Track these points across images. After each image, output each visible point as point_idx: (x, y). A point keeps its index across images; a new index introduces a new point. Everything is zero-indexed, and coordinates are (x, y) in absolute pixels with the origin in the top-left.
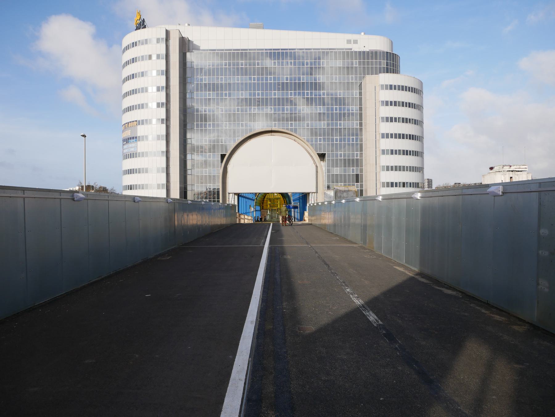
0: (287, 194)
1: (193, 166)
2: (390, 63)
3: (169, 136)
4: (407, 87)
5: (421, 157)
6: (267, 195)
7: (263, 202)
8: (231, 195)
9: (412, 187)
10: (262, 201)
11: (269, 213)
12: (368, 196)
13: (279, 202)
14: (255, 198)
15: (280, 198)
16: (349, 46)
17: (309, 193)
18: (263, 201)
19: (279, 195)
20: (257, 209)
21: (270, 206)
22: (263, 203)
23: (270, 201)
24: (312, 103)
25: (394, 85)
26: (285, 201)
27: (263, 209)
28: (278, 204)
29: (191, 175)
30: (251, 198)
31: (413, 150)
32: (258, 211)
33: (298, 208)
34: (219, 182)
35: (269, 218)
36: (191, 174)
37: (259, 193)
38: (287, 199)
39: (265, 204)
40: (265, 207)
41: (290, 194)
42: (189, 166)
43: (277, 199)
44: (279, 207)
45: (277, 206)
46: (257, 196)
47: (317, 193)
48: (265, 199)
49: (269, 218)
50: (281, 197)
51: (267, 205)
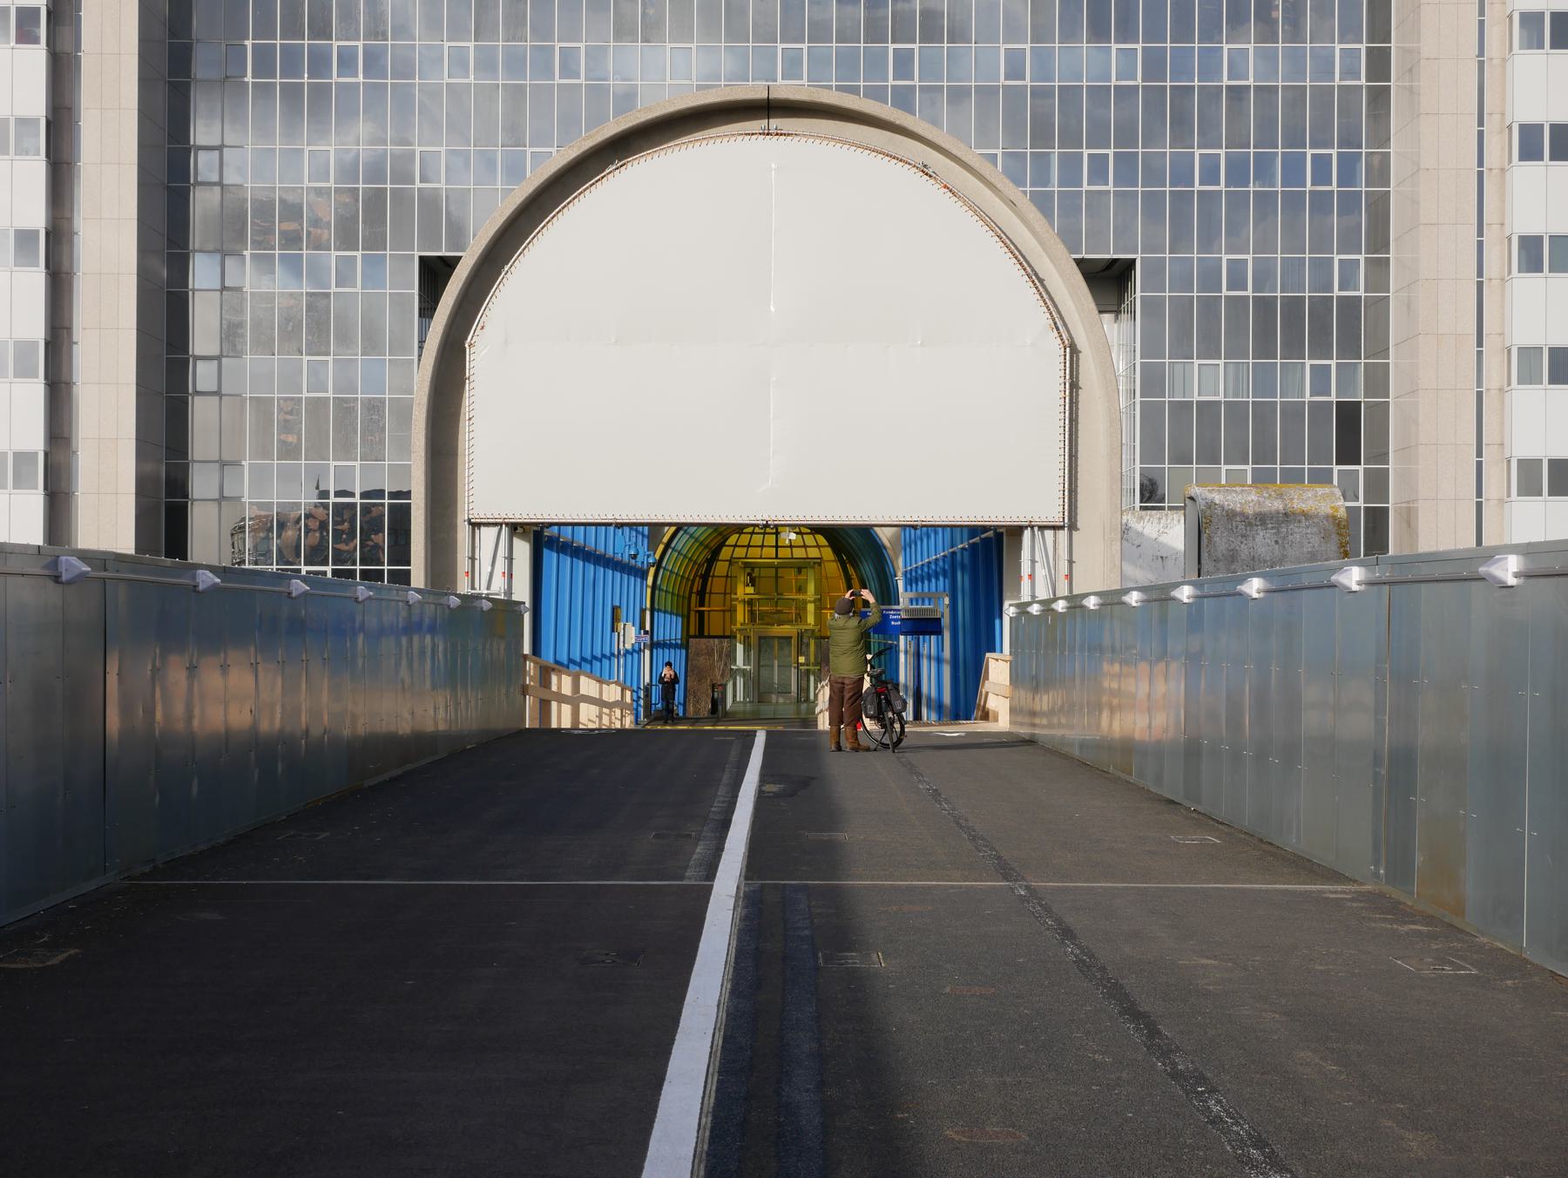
1: (230, 335)
11: (747, 660)
13: (811, 588)
14: (646, 557)
20: (660, 636)
21: (752, 613)
22: (702, 594)
23: (753, 582)
27: (701, 634)
28: (805, 602)
36: (218, 393)
39: (714, 604)
40: (714, 624)
41: (885, 535)
44: (811, 619)
45: (800, 617)
48: (720, 568)
51: (733, 610)
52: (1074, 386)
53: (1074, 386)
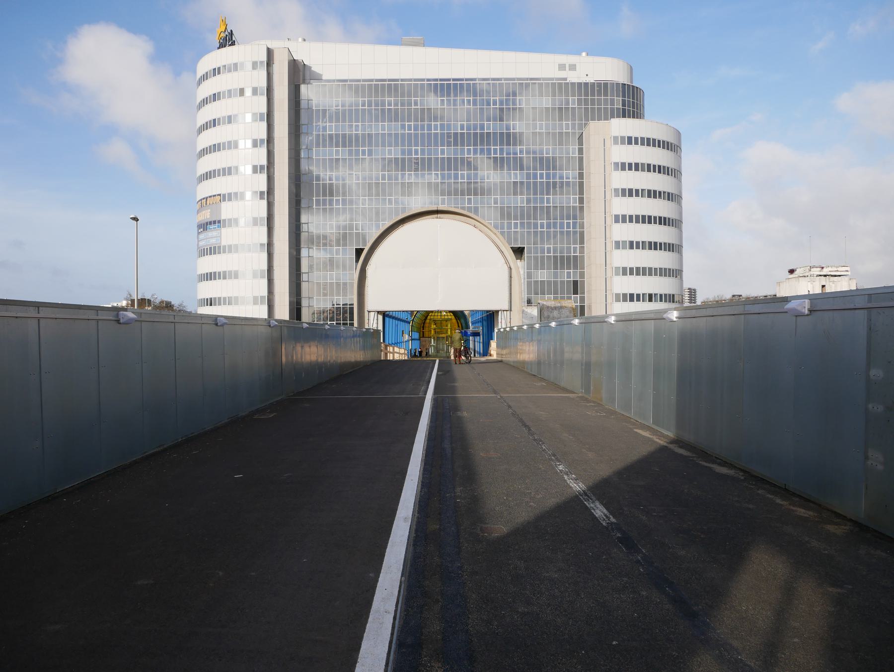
0: (462, 312)
1: (311, 267)
2: (629, 101)
3: (273, 220)
4: (656, 140)
5: (678, 253)
6: (430, 314)
7: (424, 325)
8: (372, 314)
9: (663, 301)
10: (422, 324)
11: (434, 343)
12: (593, 315)
13: (449, 326)
14: (410, 319)
15: (451, 319)
16: (562, 74)
17: (497, 312)
18: (424, 323)
19: (449, 314)
20: (413, 337)
21: (435, 331)
22: (423, 327)
23: (435, 324)
24: (503, 166)
25: (635, 138)
26: (460, 324)
27: (423, 337)
28: (448, 329)
29: (307, 283)
30: (405, 319)
31: (666, 241)
32: (416, 340)
33: (479, 336)
34: (352, 294)
35: (433, 352)
36: (308, 281)
37: (418, 311)
38: (463, 321)
39: (426, 329)
40: (426, 334)
41: (466, 313)
42: (304, 268)
43: (446, 321)
44: (449, 333)
45: (447, 332)
46: (413, 316)
47: (511, 310)
48: (428, 321)
49: (433, 352)
50: (453, 317)
51: (431, 331)
52: (511, 277)
53: (511, 277)
